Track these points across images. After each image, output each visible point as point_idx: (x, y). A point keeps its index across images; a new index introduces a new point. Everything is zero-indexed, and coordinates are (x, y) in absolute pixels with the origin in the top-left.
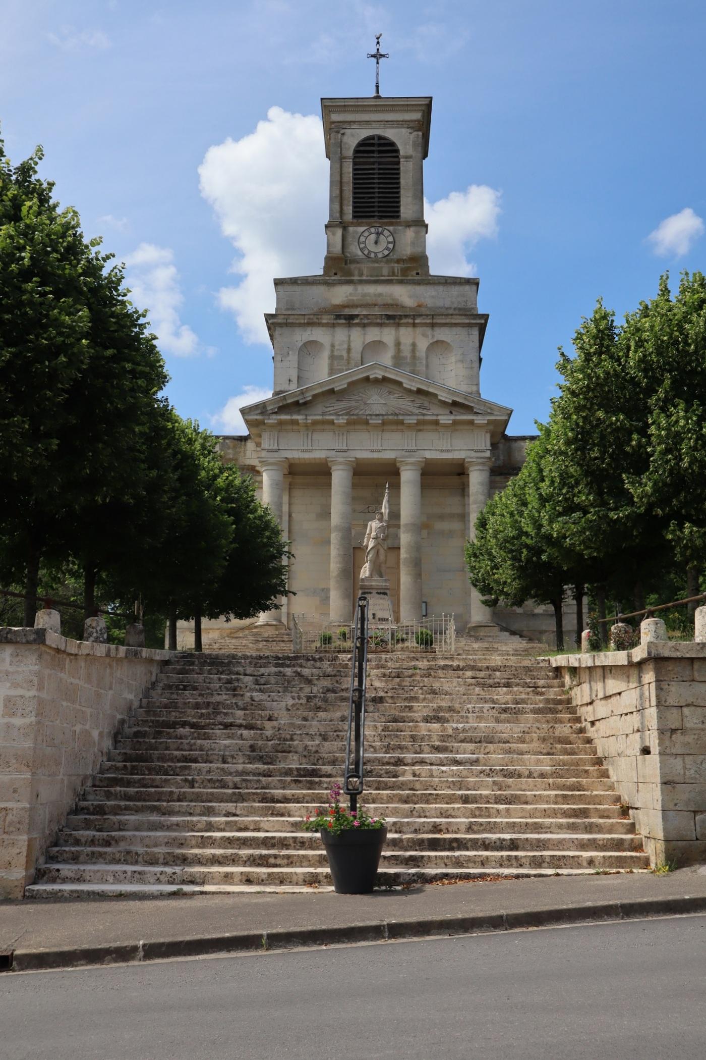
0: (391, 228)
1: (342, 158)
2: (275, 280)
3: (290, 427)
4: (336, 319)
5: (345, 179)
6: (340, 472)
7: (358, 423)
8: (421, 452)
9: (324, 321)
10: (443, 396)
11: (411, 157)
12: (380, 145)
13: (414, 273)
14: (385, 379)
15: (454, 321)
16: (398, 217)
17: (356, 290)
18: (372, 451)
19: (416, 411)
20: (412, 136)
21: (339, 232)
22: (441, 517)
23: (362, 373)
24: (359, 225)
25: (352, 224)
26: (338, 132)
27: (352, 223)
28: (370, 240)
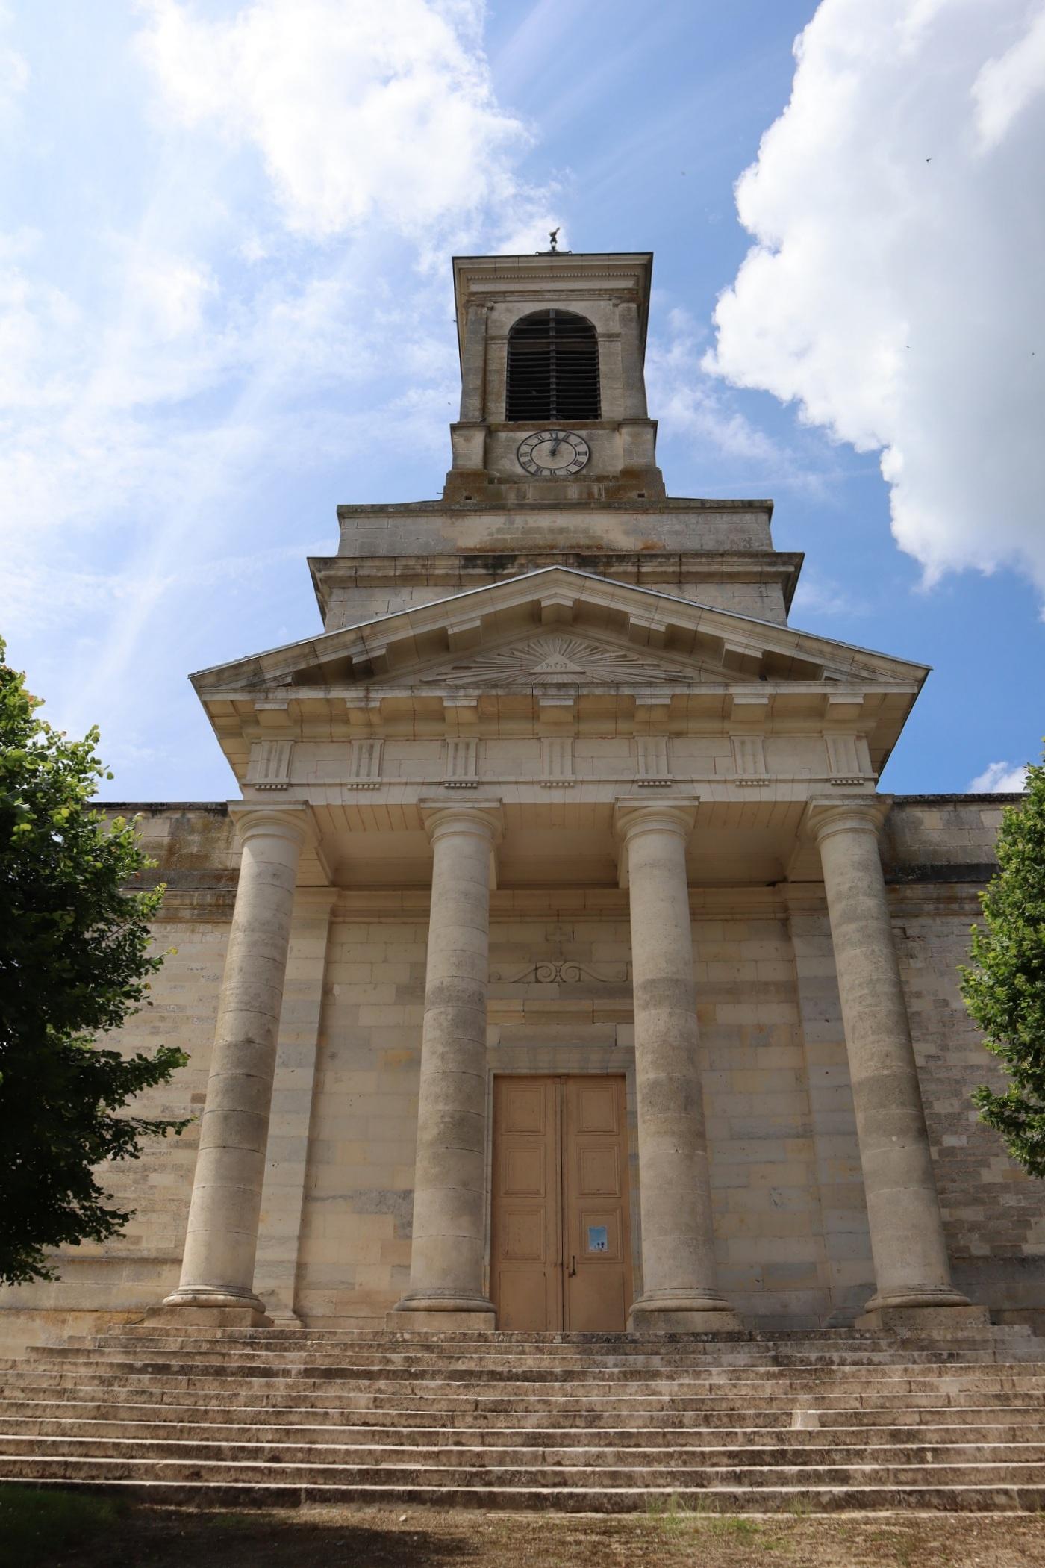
0: (584, 433)
1: (488, 340)
2: (340, 507)
3: (324, 729)
4: (465, 567)
5: (492, 366)
6: (457, 841)
7: (513, 710)
8: (682, 786)
9: (439, 572)
11: (618, 336)
13: (634, 494)
15: (727, 569)
17: (512, 523)
18: (548, 785)
20: (617, 311)
21: (479, 437)
22: (734, 992)
24: (519, 429)
25: (505, 428)
26: (483, 306)
27: (505, 426)
28: (542, 451)
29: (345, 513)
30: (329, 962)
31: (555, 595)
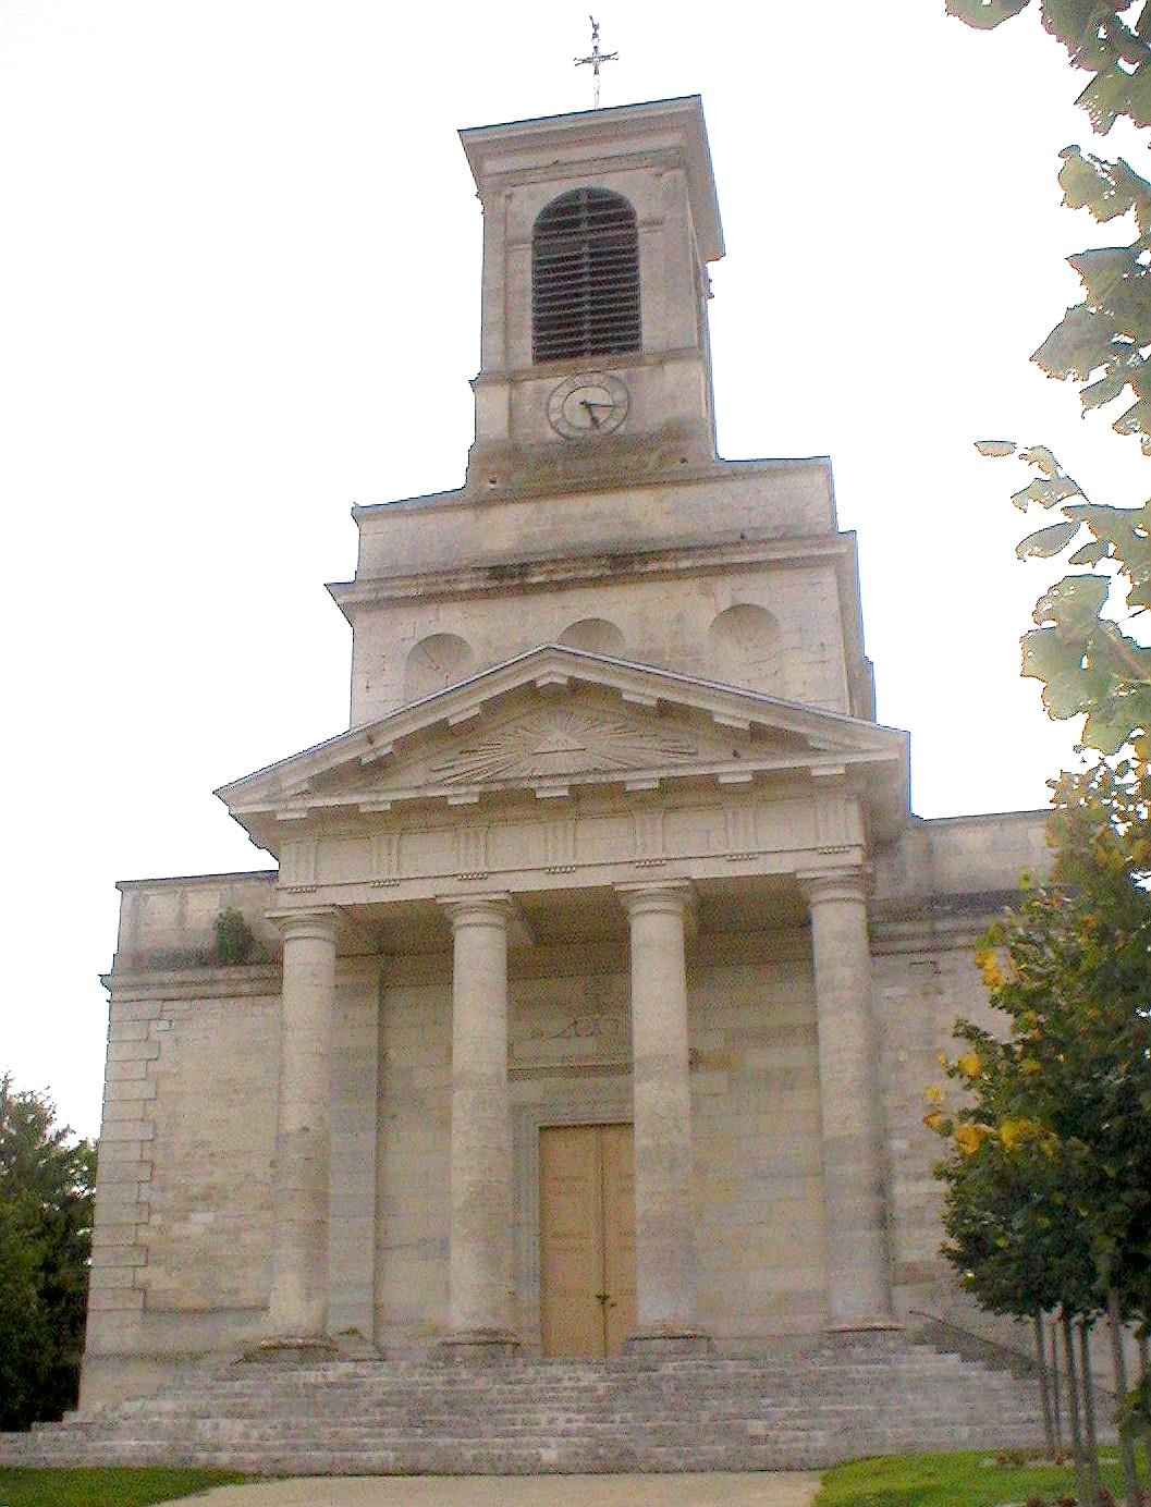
7: (506, 803)
10: (728, 715)
12: (592, 207)
14: (576, 687)
16: (635, 347)
18: (552, 871)
19: (661, 760)
23: (517, 674)
28: (574, 397)
29: (361, 515)
30: (382, 1027)
31: (549, 674)
